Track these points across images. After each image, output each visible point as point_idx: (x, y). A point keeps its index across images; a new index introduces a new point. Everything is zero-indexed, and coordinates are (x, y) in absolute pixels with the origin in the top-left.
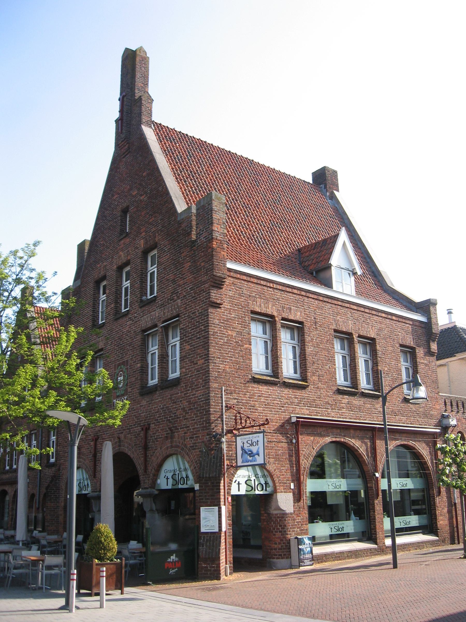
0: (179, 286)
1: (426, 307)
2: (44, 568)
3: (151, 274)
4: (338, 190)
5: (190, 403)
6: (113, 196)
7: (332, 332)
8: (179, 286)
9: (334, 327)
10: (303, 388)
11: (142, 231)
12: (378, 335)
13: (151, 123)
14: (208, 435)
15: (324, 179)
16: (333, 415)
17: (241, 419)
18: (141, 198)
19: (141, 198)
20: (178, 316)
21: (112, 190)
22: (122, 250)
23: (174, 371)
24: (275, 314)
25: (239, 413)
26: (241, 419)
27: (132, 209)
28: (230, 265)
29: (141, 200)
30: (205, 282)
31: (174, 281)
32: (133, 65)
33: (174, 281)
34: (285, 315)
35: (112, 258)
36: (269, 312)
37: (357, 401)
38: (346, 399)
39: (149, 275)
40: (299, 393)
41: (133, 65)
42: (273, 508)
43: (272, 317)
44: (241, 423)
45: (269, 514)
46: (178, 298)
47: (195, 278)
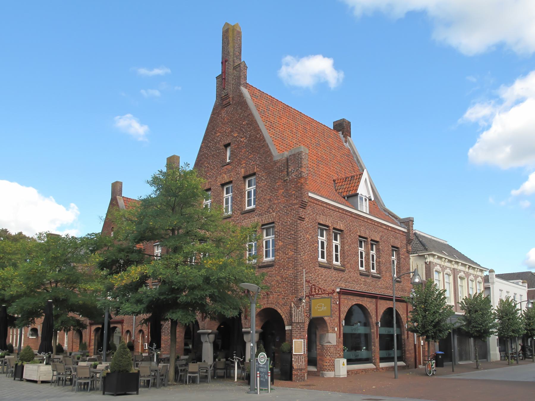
0: (274, 204)
1: (408, 222)
2: (478, 357)
3: (248, 192)
4: (350, 137)
5: (282, 277)
6: (215, 133)
7: (358, 237)
8: (274, 204)
9: (359, 234)
10: (343, 271)
11: (242, 162)
12: (381, 239)
13: (247, 86)
14: (296, 297)
15: (343, 127)
16: (357, 288)
17: (315, 289)
18: (242, 140)
19: (242, 140)
20: (273, 223)
21: (214, 129)
22: (225, 174)
23: (267, 256)
24: (330, 225)
25: (314, 285)
26: (315, 289)
27: (233, 145)
28: (310, 195)
29: (241, 141)
30: (296, 204)
31: (270, 200)
32: (230, 38)
33: (270, 200)
34: (335, 226)
35: (216, 178)
36: (327, 223)
37: (369, 280)
38: (363, 279)
39: (247, 192)
40: (341, 274)
41: (230, 38)
42: (326, 341)
43: (328, 226)
44: (315, 291)
45: (322, 345)
46: (274, 211)
47: (287, 201)
